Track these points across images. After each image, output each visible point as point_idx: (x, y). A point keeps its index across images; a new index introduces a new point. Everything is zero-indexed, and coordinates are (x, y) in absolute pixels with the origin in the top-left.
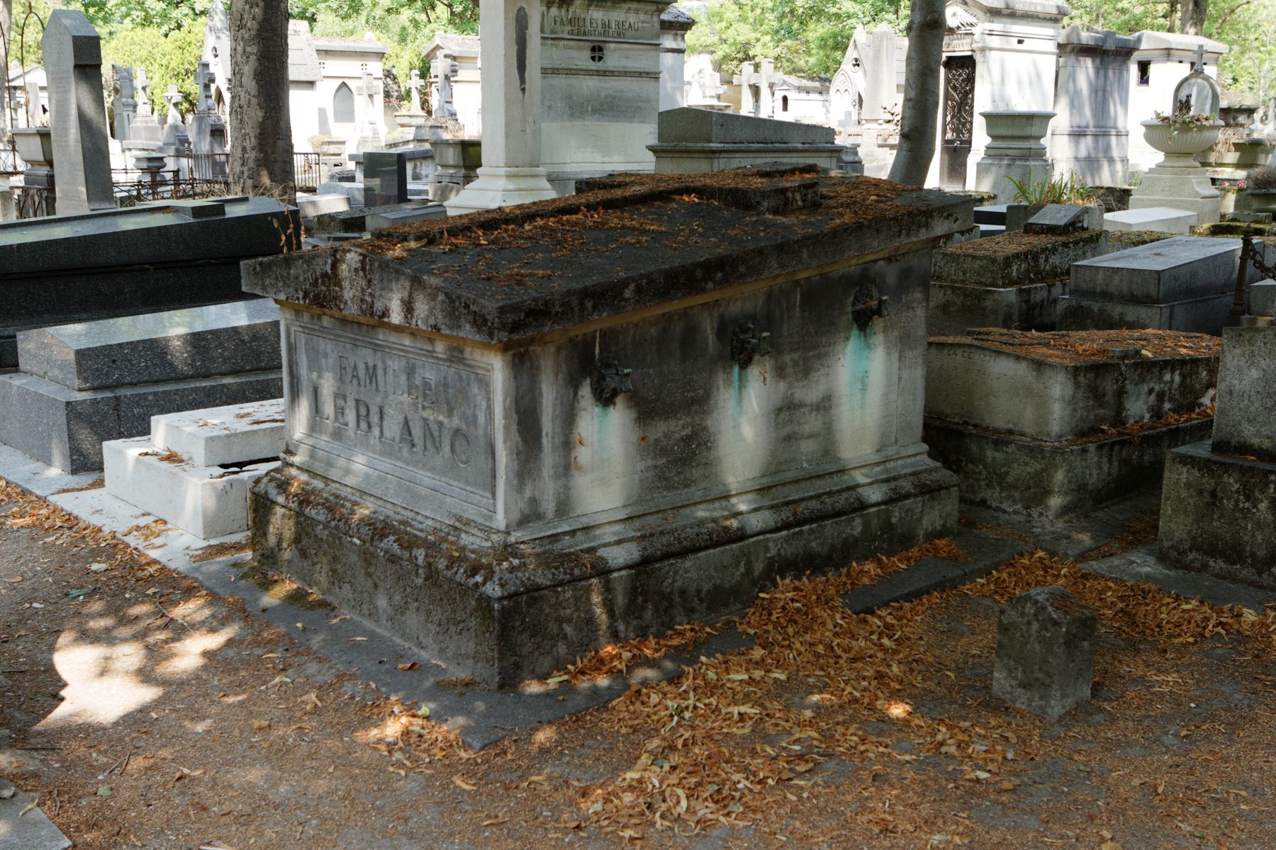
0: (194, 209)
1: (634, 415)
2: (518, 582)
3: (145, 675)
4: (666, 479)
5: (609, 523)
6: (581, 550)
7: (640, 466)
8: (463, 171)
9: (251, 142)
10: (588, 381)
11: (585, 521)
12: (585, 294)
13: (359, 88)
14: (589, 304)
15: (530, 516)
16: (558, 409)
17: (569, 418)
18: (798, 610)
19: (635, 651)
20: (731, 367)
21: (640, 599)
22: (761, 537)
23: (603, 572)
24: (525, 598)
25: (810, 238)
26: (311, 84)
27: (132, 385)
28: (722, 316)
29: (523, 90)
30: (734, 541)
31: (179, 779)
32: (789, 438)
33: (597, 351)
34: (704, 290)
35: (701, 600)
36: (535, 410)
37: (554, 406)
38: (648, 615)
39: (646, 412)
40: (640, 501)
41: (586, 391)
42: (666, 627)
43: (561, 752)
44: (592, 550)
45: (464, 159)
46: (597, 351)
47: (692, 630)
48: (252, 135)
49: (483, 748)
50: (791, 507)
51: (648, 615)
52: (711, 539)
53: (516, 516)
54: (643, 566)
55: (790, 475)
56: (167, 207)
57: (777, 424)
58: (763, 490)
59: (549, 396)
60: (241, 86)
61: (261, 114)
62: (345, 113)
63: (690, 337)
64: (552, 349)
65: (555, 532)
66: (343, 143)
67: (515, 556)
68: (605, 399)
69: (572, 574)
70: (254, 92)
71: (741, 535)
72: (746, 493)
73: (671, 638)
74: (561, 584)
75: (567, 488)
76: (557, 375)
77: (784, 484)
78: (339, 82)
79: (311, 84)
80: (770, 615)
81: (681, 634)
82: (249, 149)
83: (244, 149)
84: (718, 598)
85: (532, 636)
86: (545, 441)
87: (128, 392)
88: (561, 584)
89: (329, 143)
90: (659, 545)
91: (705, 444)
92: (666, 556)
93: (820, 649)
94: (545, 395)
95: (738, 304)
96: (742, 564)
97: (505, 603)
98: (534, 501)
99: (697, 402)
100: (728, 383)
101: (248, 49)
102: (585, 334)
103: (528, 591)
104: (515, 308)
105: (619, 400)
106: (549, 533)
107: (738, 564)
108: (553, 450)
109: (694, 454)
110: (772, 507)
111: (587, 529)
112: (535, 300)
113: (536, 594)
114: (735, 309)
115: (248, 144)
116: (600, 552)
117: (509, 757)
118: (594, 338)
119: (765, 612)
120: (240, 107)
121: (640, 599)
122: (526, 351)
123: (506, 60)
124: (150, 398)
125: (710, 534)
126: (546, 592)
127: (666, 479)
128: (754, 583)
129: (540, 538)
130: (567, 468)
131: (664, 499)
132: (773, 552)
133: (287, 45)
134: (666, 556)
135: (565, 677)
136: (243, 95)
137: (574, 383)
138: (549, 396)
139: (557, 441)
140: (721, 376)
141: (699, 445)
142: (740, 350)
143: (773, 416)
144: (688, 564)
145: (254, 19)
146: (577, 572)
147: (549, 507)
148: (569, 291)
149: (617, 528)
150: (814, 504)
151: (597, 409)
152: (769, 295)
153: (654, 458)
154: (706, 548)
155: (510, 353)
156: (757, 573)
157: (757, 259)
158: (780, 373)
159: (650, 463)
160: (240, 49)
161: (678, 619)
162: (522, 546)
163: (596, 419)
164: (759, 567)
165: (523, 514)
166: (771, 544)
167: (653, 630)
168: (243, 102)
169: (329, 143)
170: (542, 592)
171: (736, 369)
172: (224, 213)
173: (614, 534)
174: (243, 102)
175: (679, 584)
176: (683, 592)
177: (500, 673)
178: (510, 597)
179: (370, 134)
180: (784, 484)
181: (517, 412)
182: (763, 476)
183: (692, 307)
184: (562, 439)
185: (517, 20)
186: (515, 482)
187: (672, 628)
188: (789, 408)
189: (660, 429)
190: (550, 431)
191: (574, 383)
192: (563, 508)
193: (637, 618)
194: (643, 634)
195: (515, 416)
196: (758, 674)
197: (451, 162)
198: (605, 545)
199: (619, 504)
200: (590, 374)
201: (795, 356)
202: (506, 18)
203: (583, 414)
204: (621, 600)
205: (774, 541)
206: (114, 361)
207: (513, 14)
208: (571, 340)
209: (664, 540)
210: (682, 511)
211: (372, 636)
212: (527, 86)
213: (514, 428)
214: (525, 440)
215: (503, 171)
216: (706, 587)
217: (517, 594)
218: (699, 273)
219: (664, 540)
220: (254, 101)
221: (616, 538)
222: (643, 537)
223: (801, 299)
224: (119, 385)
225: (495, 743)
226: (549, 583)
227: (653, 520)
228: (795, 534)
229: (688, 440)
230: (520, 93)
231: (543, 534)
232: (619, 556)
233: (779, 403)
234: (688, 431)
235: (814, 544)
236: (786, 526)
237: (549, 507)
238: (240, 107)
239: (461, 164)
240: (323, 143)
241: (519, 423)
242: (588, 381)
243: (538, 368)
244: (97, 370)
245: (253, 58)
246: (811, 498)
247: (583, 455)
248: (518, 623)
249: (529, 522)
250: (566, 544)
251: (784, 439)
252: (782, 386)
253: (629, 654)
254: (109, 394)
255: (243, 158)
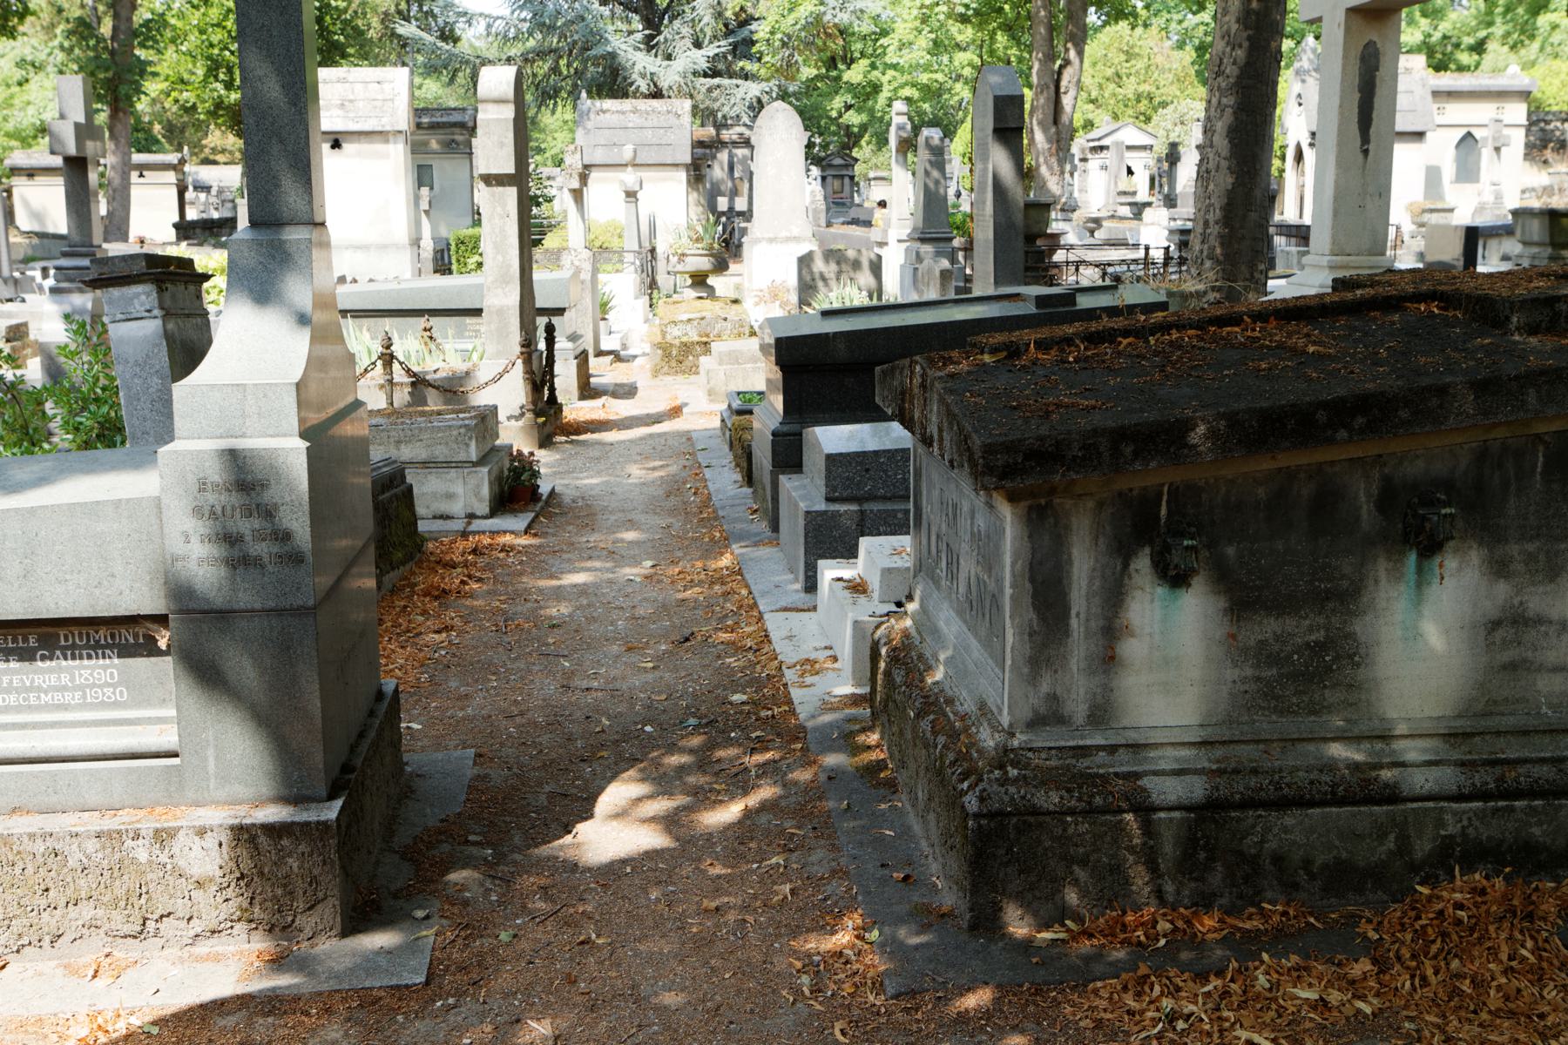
0: (1037, 297)
1: (1222, 603)
2: (1006, 798)
3: (669, 822)
4: (1277, 698)
5: (1173, 744)
6: (1116, 774)
7: (1231, 674)
8: (1550, 250)
9: (1215, 215)
10: (1147, 550)
11: (1133, 736)
12: (1120, 435)
13: (1485, 139)
14: (1128, 450)
15: (1049, 716)
16: (1097, 583)
17: (1114, 596)
18: (1459, 922)
19: (1180, 924)
20: (1403, 554)
21: (1202, 855)
22: (1431, 804)
23: (1145, 809)
24: (1015, 820)
25: (1543, 373)
26: (1419, 136)
27: (885, 498)
28: (1387, 481)
29: (1366, 152)
30: (1379, 803)
31: (582, 943)
32: (1512, 667)
33: (1164, 511)
34: (1331, 441)
35: (1312, 877)
36: (1060, 581)
37: (1091, 579)
38: (1216, 879)
39: (1242, 599)
40: (1230, 721)
41: (1142, 563)
42: (1247, 898)
43: (982, 1028)
44: (1137, 776)
45: (1552, 235)
46: (1164, 511)
47: (1285, 914)
48: (1217, 206)
49: (896, 997)
50: (1498, 770)
51: (1216, 879)
52: (1333, 793)
53: (1025, 713)
54: (1207, 811)
55: (1509, 722)
56: (1018, 295)
57: (1489, 645)
58: (1452, 737)
59: (1083, 567)
60: (1211, 146)
61: (1230, 180)
62: (1467, 171)
63: (1326, 507)
64: (1091, 504)
65: (1081, 743)
66: (1451, 210)
67: (1015, 764)
68: (1176, 579)
69: (1089, 803)
70: (1225, 152)
71: (1391, 795)
72: (1421, 736)
73: (1250, 918)
74: (1072, 812)
75: (1107, 689)
76: (1096, 538)
77: (1498, 733)
78: (1462, 132)
79: (1419, 136)
80: (1418, 918)
81: (1265, 915)
82: (1211, 223)
83: (1206, 223)
84: (1343, 878)
85: (1021, 872)
86: (1074, 622)
87: (875, 506)
88: (1072, 812)
89: (1432, 211)
90: (1239, 787)
91: (1351, 657)
92: (1247, 804)
93: (1466, 986)
94: (1076, 564)
95: (1420, 463)
96: (1392, 837)
97: (984, 822)
98: (1053, 698)
99: (1344, 597)
100: (1396, 576)
101: (1224, 101)
102: (1145, 488)
103: (1018, 813)
104: (1009, 448)
105: (1199, 584)
106: (1071, 743)
107: (1382, 836)
108: (1088, 635)
109: (1329, 669)
110: (1463, 764)
111: (1135, 747)
112: (1041, 439)
113: (1032, 819)
114: (1414, 469)
115: (1211, 217)
116: (1145, 782)
117: (919, 1016)
118: (1160, 495)
119: (1413, 914)
120: (1208, 172)
121: (1202, 855)
122: (1049, 505)
123: (1341, 114)
124: (900, 515)
125: (1334, 785)
126: (1048, 819)
127: (1277, 698)
128: (1414, 868)
129: (1059, 749)
130: (1108, 661)
131: (1267, 725)
132: (1452, 829)
133: (1275, 93)
134: (1247, 804)
135: (1062, 936)
136: (1211, 156)
137: (1123, 551)
138: (1083, 567)
139: (1093, 624)
140: (1382, 567)
141: (1337, 658)
142: (1417, 530)
143: (1483, 633)
144: (1289, 821)
145: (1234, 63)
146: (1098, 800)
147: (1078, 708)
148: (1095, 430)
149: (1185, 752)
150: (1545, 772)
151: (1159, 590)
152: (1482, 455)
153: (1257, 666)
154: (1323, 803)
155: (1024, 504)
156: (1418, 855)
157: (1435, 402)
158: (1499, 568)
159: (1249, 672)
160: (1214, 101)
161: (1269, 894)
162: (1030, 754)
163: (1157, 604)
164: (1423, 847)
165: (1035, 712)
166: (1448, 817)
167: (1224, 901)
168: (1211, 166)
169: (1432, 211)
170: (1041, 818)
171: (1412, 558)
172: (1074, 304)
173: (1177, 760)
174: (1211, 166)
175: (1272, 845)
176: (1278, 859)
177: (971, 910)
178: (991, 815)
179: (1492, 199)
180: (1498, 733)
181: (1032, 580)
182: (1459, 716)
183: (1332, 463)
184: (1101, 623)
185: (1363, 59)
186: (1026, 670)
187: (1257, 905)
188: (1515, 622)
189: (1267, 627)
190: (1083, 610)
191: (1123, 551)
192: (1100, 714)
193: (1196, 880)
194: (1204, 902)
195: (1028, 585)
196: (1335, 997)
197: (1536, 238)
198: (1155, 773)
199: (1193, 720)
200: (1151, 543)
201: (1531, 547)
202: (1345, 57)
203: (1138, 593)
204: (1169, 848)
205: (1455, 813)
206: (867, 470)
207: (1356, 52)
208: (1120, 494)
209: (1253, 782)
210: (1299, 746)
211: (905, 833)
212: (1372, 147)
213: (1028, 600)
214: (1042, 618)
215: (1325, 261)
216: (1320, 859)
217: (1000, 814)
218: (1321, 416)
219: (1253, 782)
220: (1224, 164)
221: (1176, 766)
222: (1221, 772)
223: (1545, 464)
224: (872, 497)
225: (913, 993)
226: (1052, 808)
227: (1245, 751)
228: (1496, 810)
229: (1319, 648)
230: (1360, 156)
231: (1063, 743)
232: (1167, 790)
233: (1494, 614)
234: (1319, 636)
235: (1536, 831)
236: (1484, 796)
237: (1078, 708)
238: (1208, 172)
239: (1547, 240)
240: (1424, 211)
241: (1035, 596)
242: (1147, 550)
243: (1068, 528)
244: (848, 478)
245: (1229, 110)
246: (1543, 761)
247: (1132, 649)
248: (1002, 852)
249: (1045, 724)
250: (1099, 763)
251: (1504, 667)
252: (1502, 589)
253: (1168, 926)
254: (854, 507)
255: (1203, 234)
